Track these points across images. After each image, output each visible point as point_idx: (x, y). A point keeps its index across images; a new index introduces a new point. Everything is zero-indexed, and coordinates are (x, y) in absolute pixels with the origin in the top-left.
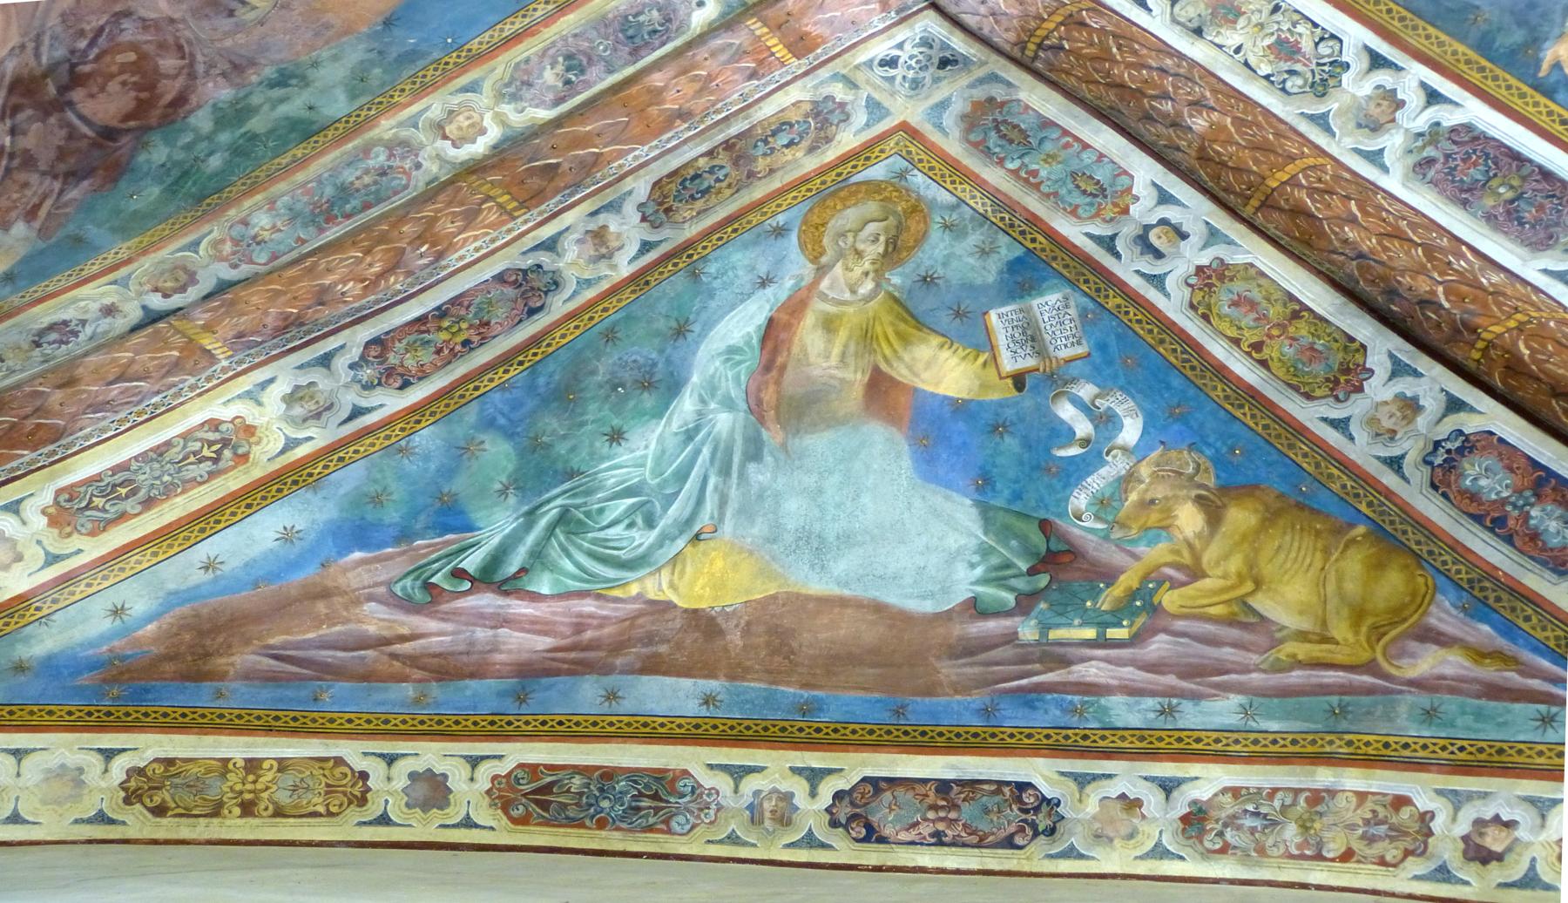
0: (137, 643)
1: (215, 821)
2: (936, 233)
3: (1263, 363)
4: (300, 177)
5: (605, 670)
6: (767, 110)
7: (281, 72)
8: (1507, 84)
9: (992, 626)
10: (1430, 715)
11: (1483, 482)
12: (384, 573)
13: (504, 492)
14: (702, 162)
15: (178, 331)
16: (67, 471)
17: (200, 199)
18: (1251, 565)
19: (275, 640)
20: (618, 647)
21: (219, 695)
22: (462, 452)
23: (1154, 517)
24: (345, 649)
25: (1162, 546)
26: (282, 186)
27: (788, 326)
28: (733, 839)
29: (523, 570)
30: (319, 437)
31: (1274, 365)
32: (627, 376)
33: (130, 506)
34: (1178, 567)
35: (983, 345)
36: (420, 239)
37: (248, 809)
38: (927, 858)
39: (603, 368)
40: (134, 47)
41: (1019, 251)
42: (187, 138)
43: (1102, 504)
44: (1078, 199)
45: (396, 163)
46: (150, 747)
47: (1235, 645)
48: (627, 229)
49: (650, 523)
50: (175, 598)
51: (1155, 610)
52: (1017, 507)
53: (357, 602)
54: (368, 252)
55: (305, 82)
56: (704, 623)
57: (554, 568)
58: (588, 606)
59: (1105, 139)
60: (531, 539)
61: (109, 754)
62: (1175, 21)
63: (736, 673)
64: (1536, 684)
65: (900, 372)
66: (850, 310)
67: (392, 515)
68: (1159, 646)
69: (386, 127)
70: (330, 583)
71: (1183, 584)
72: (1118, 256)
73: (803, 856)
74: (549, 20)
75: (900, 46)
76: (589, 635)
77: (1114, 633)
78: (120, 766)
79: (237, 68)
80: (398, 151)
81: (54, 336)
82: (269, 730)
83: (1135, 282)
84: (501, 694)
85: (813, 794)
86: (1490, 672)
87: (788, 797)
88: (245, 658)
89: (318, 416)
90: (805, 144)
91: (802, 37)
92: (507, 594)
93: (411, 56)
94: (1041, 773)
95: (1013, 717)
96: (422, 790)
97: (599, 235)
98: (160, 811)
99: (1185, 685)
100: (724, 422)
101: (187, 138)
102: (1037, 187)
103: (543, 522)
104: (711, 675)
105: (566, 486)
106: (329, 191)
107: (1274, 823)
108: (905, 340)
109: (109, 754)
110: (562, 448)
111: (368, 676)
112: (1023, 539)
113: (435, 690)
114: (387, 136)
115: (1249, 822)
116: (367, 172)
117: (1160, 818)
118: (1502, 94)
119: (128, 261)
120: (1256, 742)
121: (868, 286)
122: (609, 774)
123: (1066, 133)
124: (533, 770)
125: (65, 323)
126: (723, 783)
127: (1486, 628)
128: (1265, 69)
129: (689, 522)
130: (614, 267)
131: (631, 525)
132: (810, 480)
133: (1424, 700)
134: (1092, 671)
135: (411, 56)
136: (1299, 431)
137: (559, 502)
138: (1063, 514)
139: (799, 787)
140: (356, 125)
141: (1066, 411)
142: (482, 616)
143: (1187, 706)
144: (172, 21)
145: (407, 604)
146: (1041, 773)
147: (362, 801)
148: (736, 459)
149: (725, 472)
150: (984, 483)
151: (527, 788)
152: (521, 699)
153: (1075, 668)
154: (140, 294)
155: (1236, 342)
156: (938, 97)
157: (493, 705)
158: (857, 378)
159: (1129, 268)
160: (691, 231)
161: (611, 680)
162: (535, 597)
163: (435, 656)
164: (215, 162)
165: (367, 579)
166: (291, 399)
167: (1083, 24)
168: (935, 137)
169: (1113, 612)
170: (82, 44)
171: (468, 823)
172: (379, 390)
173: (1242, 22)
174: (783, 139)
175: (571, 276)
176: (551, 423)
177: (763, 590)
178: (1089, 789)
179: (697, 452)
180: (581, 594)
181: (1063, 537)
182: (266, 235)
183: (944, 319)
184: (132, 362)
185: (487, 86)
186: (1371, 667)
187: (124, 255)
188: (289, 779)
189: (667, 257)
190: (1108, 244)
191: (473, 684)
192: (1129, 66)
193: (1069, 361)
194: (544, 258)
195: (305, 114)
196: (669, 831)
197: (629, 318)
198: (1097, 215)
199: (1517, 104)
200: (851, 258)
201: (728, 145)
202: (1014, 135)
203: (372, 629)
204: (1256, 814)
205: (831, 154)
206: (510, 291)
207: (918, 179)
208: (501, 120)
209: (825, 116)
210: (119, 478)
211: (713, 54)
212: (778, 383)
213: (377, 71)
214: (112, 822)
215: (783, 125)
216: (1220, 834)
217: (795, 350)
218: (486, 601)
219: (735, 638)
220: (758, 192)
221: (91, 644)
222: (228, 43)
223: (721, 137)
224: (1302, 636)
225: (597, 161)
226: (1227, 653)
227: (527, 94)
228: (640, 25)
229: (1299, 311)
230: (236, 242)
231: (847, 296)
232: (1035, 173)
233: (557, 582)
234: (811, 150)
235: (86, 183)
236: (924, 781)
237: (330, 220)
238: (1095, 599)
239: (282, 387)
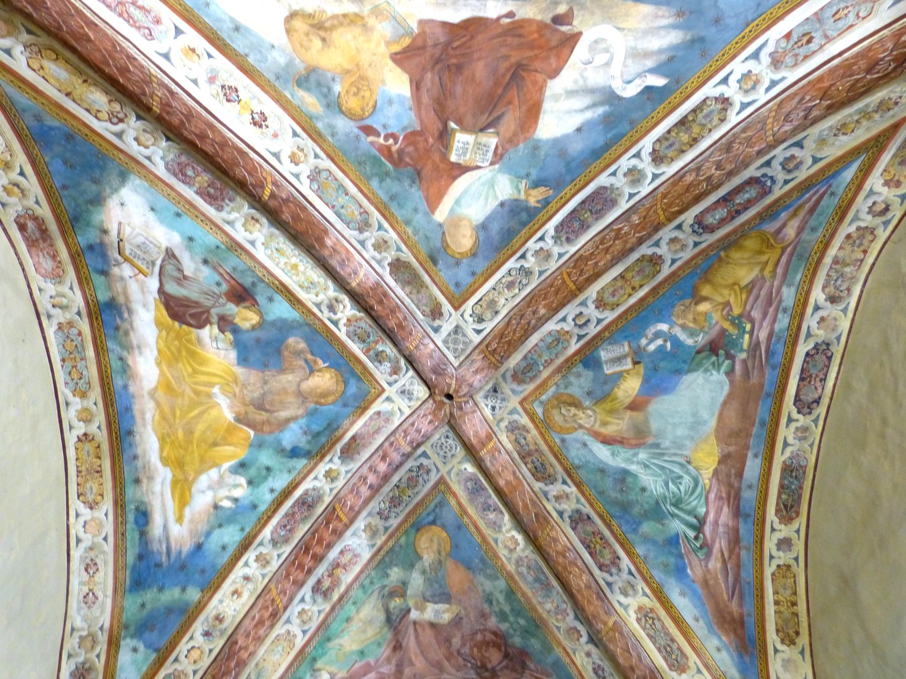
0: (731, 643)
1: (800, 614)
2: (569, 391)
3: (641, 286)
4: (530, 594)
5: (739, 489)
6: (509, 446)
7: (486, 601)
8: (541, 217)
9: (738, 367)
10: (813, 229)
11: (717, 217)
12: (696, 562)
13: (663, 525)
14: (529, 466)
15: (607, 633)
16: (662, 667)
17: (537, 626)
18: (726, 287)
19: (725, 596)
20: (730, 485)
21: (749, 615)
22: (646, 539)
23: (701, 318)
24: (728, 574)
25: (713, 315)
26: (534, 601)
27: (605, 436)
28: (811, 446)
29: (696, 517)
30: (641, 585)
31: (643, 283)
32: (618, 487)
33: (675, 646)
34: (723, 310)
35: (620, 375)
36: (564, 556)
37: (794, 604)
38: (830, 383)
39: (614, 494)
40: (471, 649)
41: (581, 365)
42: (511, 631)
43: (692, 334)
44: (560, 346)
45: (525, 564)
46: (772, 637)
47: (760, 290)
48: (554, 489)
49: (681, 477)
50: (711, 630)
51: (740, 316)
52: (689, 361)
53: (708, 571)
54: (570, 573)
55: (491, 594)
56: (724, 459)
57: (695, 508)
58: (712, 496)
59: (534, 339)
60: (682, 515)
61: (776, 651)
62: (491, 320)
63: (746, 447)
64: (814, 199)
65: (628, 401)
66: (599, 417)
67: (672, 560)
68: (756, 314)
69: (511, 568)
70: (701, 580)
71: (731, 308)
72: (586, 334)
73: (821, 423)
74: (470, 517)
75: (487, 406)
76: (724, 495)
77: (748, 327)
78: (780, 646)
79: (483, 616)
80: (520, 563)
81: (600, 672)
82: (762, 598)
83: (599, 328)
84: (746, 522)
85: (797, 420)
86: (802, 213)
87: (797, 429)
88: (734, 606)
89: (632, 586)
90: (525, 434)
91: (487, 437)
92: (705, 522)
93: (483, 561)
94: (802, 349)
95: (778, 358)
96: (784, 547)
97: (558, 498)
98: (797, 633)
99: (774, 306)
100: (643, 455)
101: (511, 631)
102: (552, 360)
103: (676, 511)
104: (746, 456)
105: (662, 505)
106: (537, 585)
107: (842, 275)
108: (615, 399)
109: (776, 651)
110: (646, 507)
111: (738, 566)
112: (703, 359)
113: (744, 543)
114: (514, 567)
115: (839, 282)
116: (529, 573)
117: (831, 311)
118: (545, 218)
119: (564, 649)
120: (804, 282)
121: (589, 412)
122: (782, 486)
123: (530, 351)
124: (778, 511)
125: (594, 669)
126: (789, 450)
127: (783, 214)
128: (517, 291)
129: (682, 465)
130: (572, 493)
131: (680, 483)
132: (670, 428)
133: (807, 231)
134: (763, 335)
135: (483, 561)
136: (673, 274)
137: (668, 507)
138: (695, 347)
139: (794, 425)
140: (509, 577)
141: (652, 347)
142: (714, 530)
143: (784, 304)
144: (463, 637)
145: (708, 555)
146: (802, 349)
147: (789, 567)
148: (658, 451)
149: (663, 454)
150: (679, 372)
151: (784, 512)
152: (748, 516)
153: (761, 340)
154: (580, 644)
155: (630, 295)
156: (510, 393)
157: (750, 525)
158: (629, 413)
159: (593, 330)
160: (559, 468)
161: (744, 486)
162: (707, 513)
163: (729, 544)
164: (522, 622)
165: (698, 568)
166: (625, 594)
167: (495, 350)
168: (526, 393)
169: (739, 329)
170: (469, 665)
171: (798, 531)
172: (621, 566)
173: (496, 299)
174: (523, 441)
175: (574, 506)
176: (636, 510)
177: (713, 440)
178: (812, 333)
179: (654, 464)
180: (707, 498)
181: (704, 346)
182: (555, 605)
183: (607, 388)
184: (622, 648)
185: (495, 536)
186: (784, 250)
187: (561, 650)
188: (781, 590)
189: (570, 476)
190: (580, 337)
191: (741, 531)
192: (514, 334)
193: (630, 347)
194: (566, 516)
195: (504, 593)
196: (806, 466)
197: (595, 487)
198: (568, 341)
199: (550, 213)
200: (576, 418)
201: (523, 458)
202: (528, 368)
203: (719, 565)
204: (836, 280)
205: (530, 425)
206: (580, 526)
207: (544, 398)
208: (508, 531)
209: (514, 428)
210: (663, 651)
211: (493, 465)
212: (628, 439)
213: (488, 571)
214: (803, 649)
215: (517, 441)
216: (841, 291)
217: (615, 434)
218: (707, 529)
219: (732, 449)
220: (544, 448)
221: (732, 657)
222: (473, 619)
223: (519, 461)
224: (762, 270)
225: (531, 500)
226: (763, 293)
227: (498, 523)
228: (473, 488)
229: (622, 276)
230: (557, 614)
231: (593, 419)
232: (546, 361)
233: (701, 506)
234: (528, 431)
235: (528, 663)
236: (798, 385)
237: (549, 584)
238: (732, 335)
239: (622, 599)
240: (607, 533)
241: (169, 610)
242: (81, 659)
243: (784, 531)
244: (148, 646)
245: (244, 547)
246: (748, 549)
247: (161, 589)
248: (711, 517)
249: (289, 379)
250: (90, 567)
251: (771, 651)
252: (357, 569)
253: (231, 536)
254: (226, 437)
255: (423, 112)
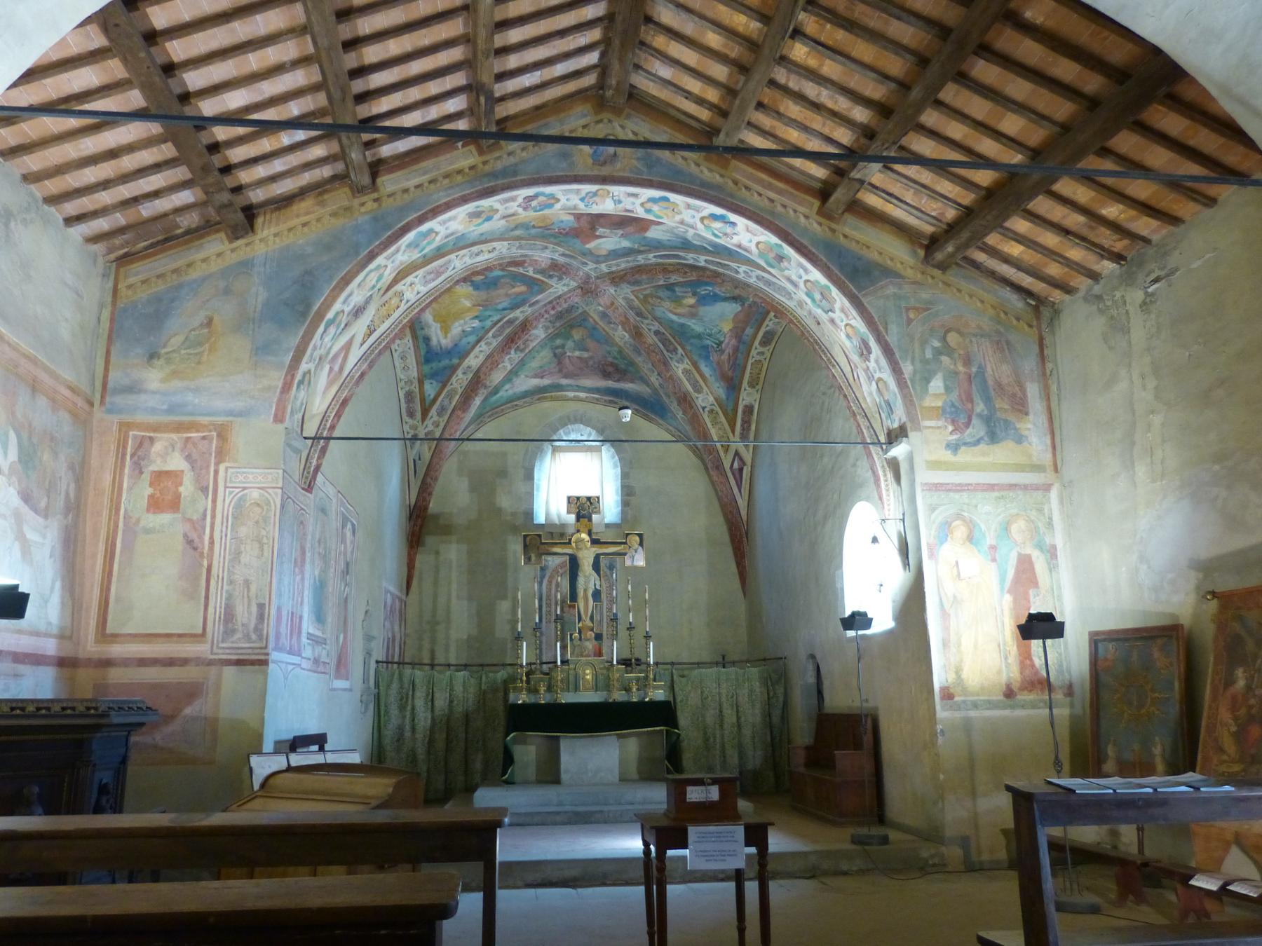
6: (624, 304)
30: (686, 360)
46: (745, 384)
78: (747, 388)
141: (703, 293)
166: (678, 363)
203: (727, 357)
218: (723, 345)
239: (676, 364)
240: (673, 340)
241: (445, 368)
242: (407, 389)
243: (761, 349)
244: (437, 381)
245: (478, 341)
246: (742, 353)
247: (440, 361)
248: (726, 341)
249: (501, 291)
250: (403, 358)
251: (743, 389)
252: (538, 341)
253: (472, 339)
254: (469, 310)
255: (608, 882)
